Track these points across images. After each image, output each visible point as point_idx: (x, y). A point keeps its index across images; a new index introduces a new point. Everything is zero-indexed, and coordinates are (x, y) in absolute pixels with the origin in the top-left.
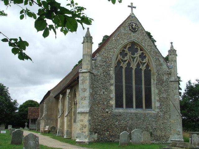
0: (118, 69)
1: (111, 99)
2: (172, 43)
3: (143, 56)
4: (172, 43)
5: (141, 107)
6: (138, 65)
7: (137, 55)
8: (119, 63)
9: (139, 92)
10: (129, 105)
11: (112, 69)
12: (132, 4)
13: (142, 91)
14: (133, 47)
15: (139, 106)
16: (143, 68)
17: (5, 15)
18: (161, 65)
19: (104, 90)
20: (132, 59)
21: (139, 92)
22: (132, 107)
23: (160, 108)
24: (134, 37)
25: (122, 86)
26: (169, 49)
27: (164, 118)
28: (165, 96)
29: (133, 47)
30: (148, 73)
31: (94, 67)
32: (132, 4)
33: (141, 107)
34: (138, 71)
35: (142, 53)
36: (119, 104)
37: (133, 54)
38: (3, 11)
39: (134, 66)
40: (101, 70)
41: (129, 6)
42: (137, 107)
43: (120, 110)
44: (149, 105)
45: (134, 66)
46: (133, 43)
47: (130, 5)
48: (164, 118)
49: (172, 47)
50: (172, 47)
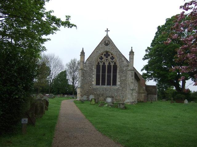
0: (98, 67)
1: (93, 81)
2: (132, 47)
3: (112, 58)
4: (132, 47)
5: (110, 85)
6: (109, 63)
7: (109, 58)
8: (98, 63)
9: (109, 77)
10: (103, 84)
11: (94, 67)
12: (107, 29)
13: (111, 77)
14: (107, 54)
15: (109, 84)
16: (112, 64)
17: (83, 51)
18: (123, 61)
19: (89, 77)
20: (106, 60)
21: (109, 77)
22: (105, 85)
23: (120, 85)
24: (107, 48)
25: (113, 73)
26: (130, 51)
27: (122, 91)
28: (124, 78)
29: (107, 54)
30: (115, 67)
31: (85, 67)
32: (106, 31)
33: (110, 85)
34: (104, 66)
35: (112, 56)
36: (98, 83)
37: (107, 57)
38: (65, 27)
39: (107, 64)
40: (88, 68)
41: (107, 29)
42: (113, 85)
43: (98, 86)
44: (115, 83)
45: (107, 64)
46: (107, 52)
47: (106, 30)
48: (122, 91)
49: (132, 50)
50: (132, 50)
